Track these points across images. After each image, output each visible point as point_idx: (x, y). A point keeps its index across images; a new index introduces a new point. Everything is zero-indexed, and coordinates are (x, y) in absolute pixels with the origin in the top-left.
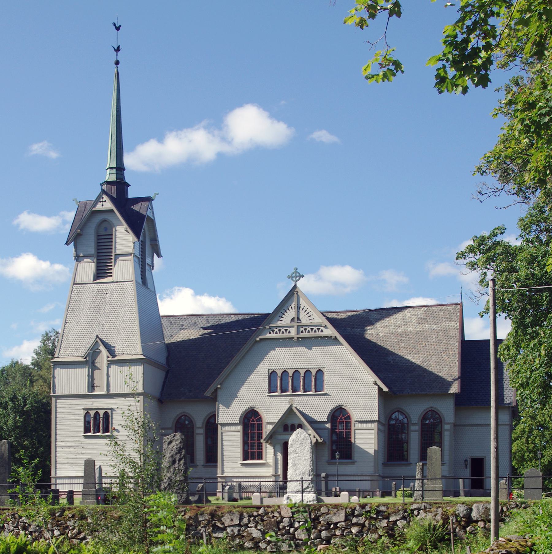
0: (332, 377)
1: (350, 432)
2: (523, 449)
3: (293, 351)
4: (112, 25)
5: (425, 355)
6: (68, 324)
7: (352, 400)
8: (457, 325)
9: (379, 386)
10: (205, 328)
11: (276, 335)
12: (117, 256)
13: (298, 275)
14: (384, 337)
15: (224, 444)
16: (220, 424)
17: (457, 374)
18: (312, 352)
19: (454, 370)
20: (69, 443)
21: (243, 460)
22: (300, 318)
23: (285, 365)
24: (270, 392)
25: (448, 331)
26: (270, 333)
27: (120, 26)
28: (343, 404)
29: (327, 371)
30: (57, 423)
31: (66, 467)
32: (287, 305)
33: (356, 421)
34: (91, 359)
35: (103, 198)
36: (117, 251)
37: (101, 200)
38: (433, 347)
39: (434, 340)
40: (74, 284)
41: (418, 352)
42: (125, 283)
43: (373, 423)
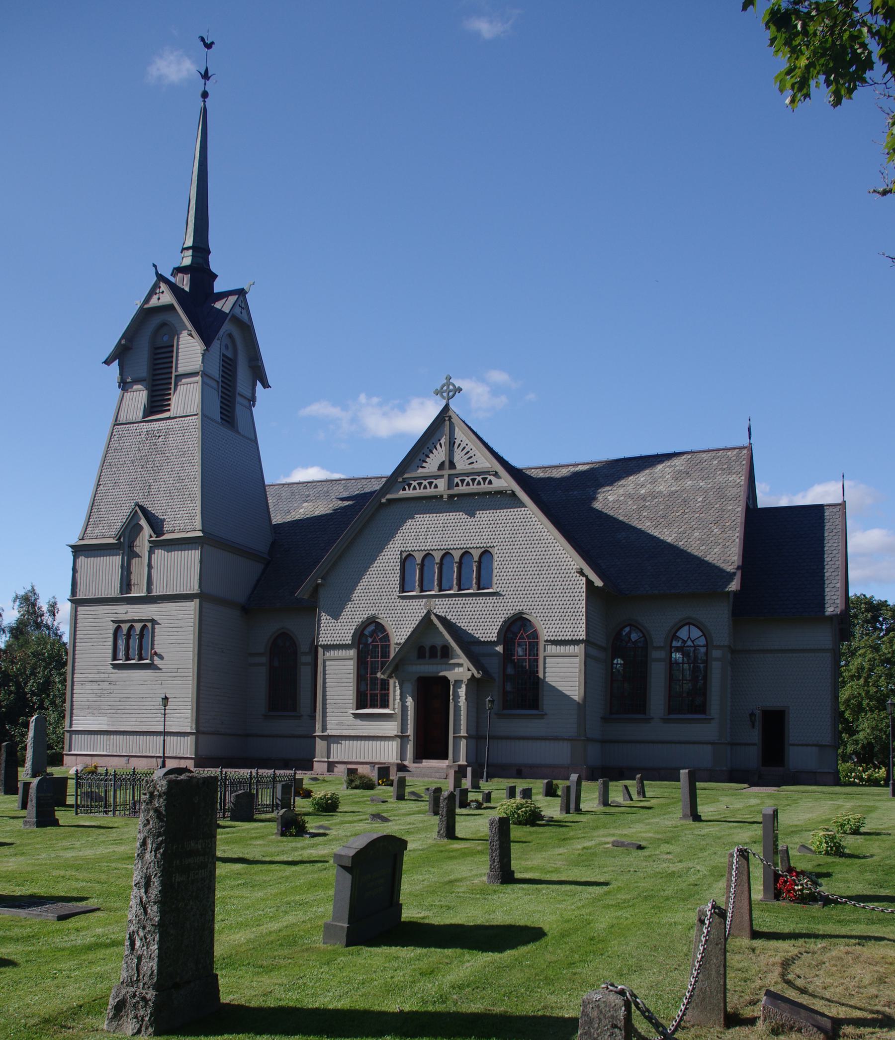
0: (507, 563)
1: (537, 661)
2: (860, 694)
3: (443, 518)
4: (199, 40)
5: (682, 529)
6: (101, 486)
7: (540, 604)
8: (742, 480)
9: (587, 577)
10: (342, 499)
11: (415, 491)
12: (179, 377)
13: (451, 387)
14: (614, 502)
15: (327, 680)
16: (322, 646)
17: (736, 558)
18: (474, 520)
19: (731, 552)
20: (91, 677)
21: (357, 709)
22: (455, 461)
23: (428, 544)
24: (403, 590)
25: (724, 490)
26: (404, 489)
27: (213, 43)
28: (525, 611)
29: (498, 552)
30: (77, 644)
31: (85, 714)
32: (433, 440)
33: (547, 641)
34: (127, 539)
35: (160, 287)
36: (179, 369)
37: (158, 292)
38: (697, 515)
39: (700, 504)
40: (117, 423)
41: (669, 525)
42: (186, 418)
43: (578, 645)
